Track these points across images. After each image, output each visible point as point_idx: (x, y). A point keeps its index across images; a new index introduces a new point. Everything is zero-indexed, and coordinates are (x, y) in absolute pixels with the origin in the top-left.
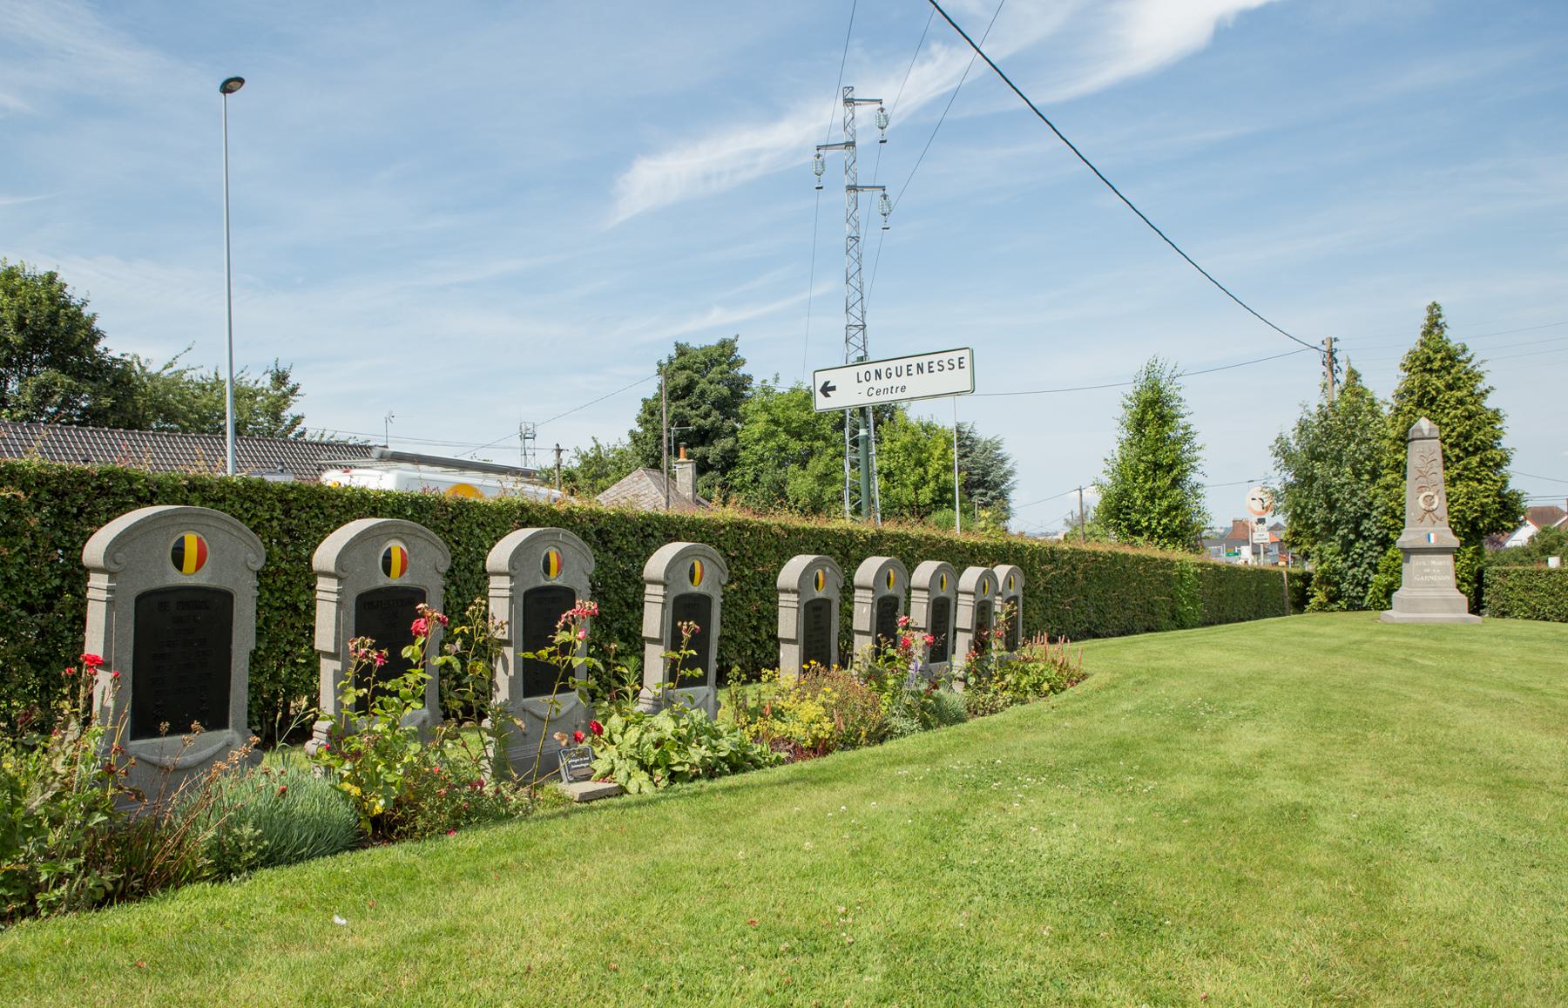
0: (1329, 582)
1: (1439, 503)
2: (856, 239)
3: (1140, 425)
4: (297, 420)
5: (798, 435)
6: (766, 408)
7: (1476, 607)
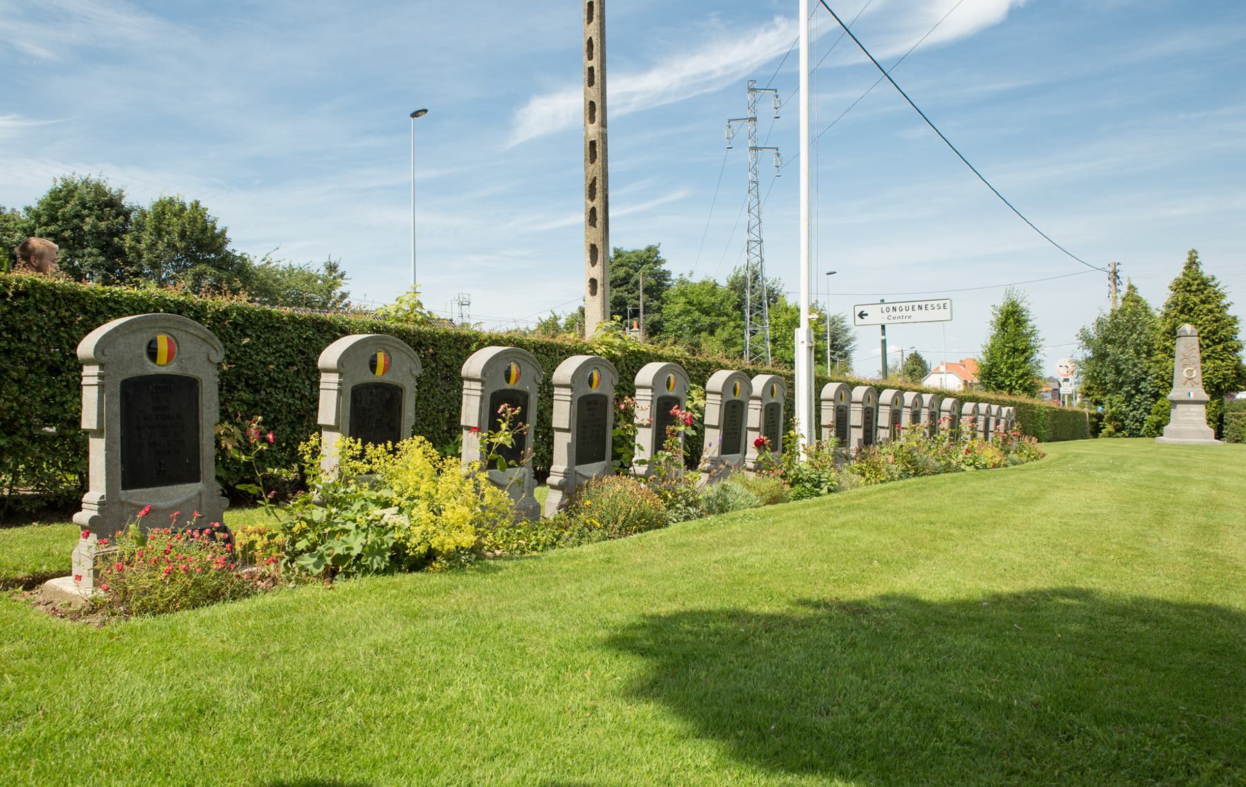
0: (1116, 419)
1: (1197, 374)
2: (757, 183)
3: (1004, 325)
4: (344, 296)
5: (706, 313)
6: (683, 294)
7: (1219, 436)
